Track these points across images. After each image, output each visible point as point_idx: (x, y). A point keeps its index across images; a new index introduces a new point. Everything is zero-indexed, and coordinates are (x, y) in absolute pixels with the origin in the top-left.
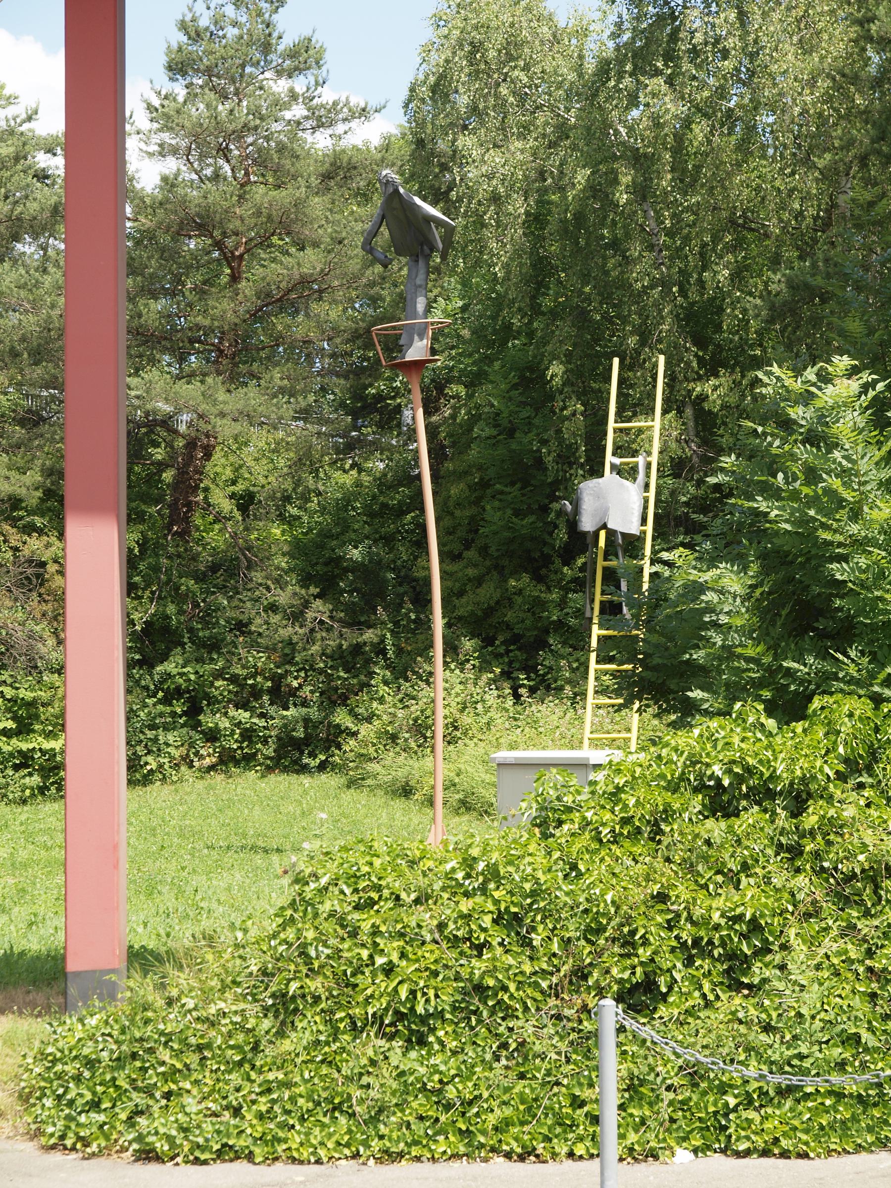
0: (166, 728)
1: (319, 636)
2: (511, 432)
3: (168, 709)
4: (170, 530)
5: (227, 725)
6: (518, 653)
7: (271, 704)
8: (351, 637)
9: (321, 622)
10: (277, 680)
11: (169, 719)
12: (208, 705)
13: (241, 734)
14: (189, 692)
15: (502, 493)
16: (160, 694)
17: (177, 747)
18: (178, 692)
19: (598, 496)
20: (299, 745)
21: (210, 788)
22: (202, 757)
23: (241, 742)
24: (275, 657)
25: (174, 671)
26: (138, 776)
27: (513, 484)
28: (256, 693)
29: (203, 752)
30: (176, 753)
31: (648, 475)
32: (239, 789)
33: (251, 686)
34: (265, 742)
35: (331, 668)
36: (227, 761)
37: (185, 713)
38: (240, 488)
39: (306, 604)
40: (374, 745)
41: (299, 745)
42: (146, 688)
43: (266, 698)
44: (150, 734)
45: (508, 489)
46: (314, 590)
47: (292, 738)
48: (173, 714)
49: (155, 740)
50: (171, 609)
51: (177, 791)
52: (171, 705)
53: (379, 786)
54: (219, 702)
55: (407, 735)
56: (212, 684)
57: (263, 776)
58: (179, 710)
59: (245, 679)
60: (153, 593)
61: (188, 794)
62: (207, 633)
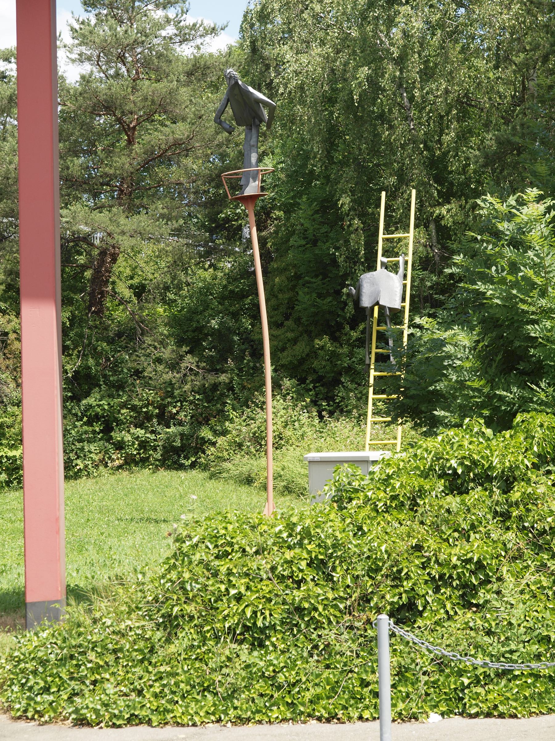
1: (189, 379)
2: (315, 243)
3: (91, 429)
4: (90, 310)
5: (130, 439)
6: (321, 388)
7: (159, 424)
8: (211, 379)
9: (191, 370)
12: (117, 425)
13: (139, 445)
14: (104, 417)
15: (309, 282)
16: (85, 419)
18: (97, 417)
19: (373, 283)
20: (177, 451)
21: (119, 480)
23: (139, 450)
25: (94, 404)
26: (71, 473)
27: (316, 276)
28: (149, 417)
29: (114, 457)
30: (96, 458)
31: (406, 269)
32: (138, 481)
33: (145, 412)
34: (155, 450)
36: (130, 462)
37: (101, 431)
38: (136, 281)
39: (181, 358)
40: (227, 450)
41: (177, 451)
42: (76, 415)
44: (79, 445)
45: (314, 280)
47: (173, 447)
48: (94, 432)
49: (82, 449)
50: (91, 362)
51: (97, 482)
53: (231, 478)
54: (124, 424)
55: (249, 444)
56: (119, 412)
57: (154, 472)
59: (141, 408)
62: (115, 378)
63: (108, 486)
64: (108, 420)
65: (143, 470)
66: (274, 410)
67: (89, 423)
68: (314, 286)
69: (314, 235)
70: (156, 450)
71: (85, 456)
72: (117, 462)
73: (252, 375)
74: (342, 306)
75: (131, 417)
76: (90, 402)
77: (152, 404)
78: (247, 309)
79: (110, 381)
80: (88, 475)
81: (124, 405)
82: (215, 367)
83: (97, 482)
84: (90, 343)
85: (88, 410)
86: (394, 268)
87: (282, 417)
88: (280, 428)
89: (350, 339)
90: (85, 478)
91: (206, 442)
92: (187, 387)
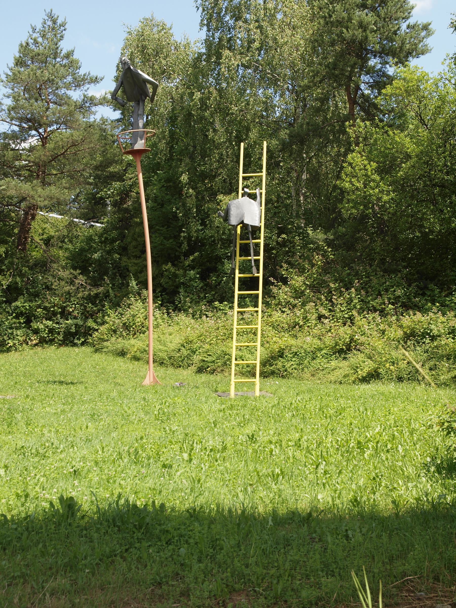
0: (17, 328)
1: (81, 290)
2: (162, 205)
3: (18, 321)
4: (17, 248)
5: (43, 327)
7: (61, 318)
8: (95, 291)
9: (82, 285)
10: (63, 308)
11: (18, 325)
12: (34, 319)
13: (48, 331)
14: (26, 314)
15: (159, 230)
16: (14, 315)
17: (21, 336)
19: (238, 207)
21: (36, 353)
22: (32, 340)
23: (49, 334)
24: (63, 299)
25: (20, 305)
26: (5, 348)
27: (163, 226)
29: (32, 338)
30: (21, 339)
31: (261, 197)
32: (48, 354)
33: (52, 311)
35: (86, 303)
36: (43, 342)
37: (24, 322)
38: (45, 236)
42: (8, 312)
43: (59, 316)
44: (10, 331)
46: (78, 271)
47: (70, 332)
48: (20, 323)
49: (12, 334)
50: (18, 279)
51: (21, 354)
52: (19, 319)
54: (39, 318)
55: (121, 330)
56: (36, 311)
57: (58, 348)
58: (22, 321)
59: (50, 308)
60: (11, 273)
61: (26, 356)
62: (33, 290)
66: (144, 308)
67: (17, 317)
68: (162, 232)
71: (14, 338)
72: (34, 341)
73: (120, 288)
74: (179, 245)
75: (43, 313)
80: (16, 350)
81: (39, 307)
86: (253, 197)
87: (142, 313)
88: (142, 320)
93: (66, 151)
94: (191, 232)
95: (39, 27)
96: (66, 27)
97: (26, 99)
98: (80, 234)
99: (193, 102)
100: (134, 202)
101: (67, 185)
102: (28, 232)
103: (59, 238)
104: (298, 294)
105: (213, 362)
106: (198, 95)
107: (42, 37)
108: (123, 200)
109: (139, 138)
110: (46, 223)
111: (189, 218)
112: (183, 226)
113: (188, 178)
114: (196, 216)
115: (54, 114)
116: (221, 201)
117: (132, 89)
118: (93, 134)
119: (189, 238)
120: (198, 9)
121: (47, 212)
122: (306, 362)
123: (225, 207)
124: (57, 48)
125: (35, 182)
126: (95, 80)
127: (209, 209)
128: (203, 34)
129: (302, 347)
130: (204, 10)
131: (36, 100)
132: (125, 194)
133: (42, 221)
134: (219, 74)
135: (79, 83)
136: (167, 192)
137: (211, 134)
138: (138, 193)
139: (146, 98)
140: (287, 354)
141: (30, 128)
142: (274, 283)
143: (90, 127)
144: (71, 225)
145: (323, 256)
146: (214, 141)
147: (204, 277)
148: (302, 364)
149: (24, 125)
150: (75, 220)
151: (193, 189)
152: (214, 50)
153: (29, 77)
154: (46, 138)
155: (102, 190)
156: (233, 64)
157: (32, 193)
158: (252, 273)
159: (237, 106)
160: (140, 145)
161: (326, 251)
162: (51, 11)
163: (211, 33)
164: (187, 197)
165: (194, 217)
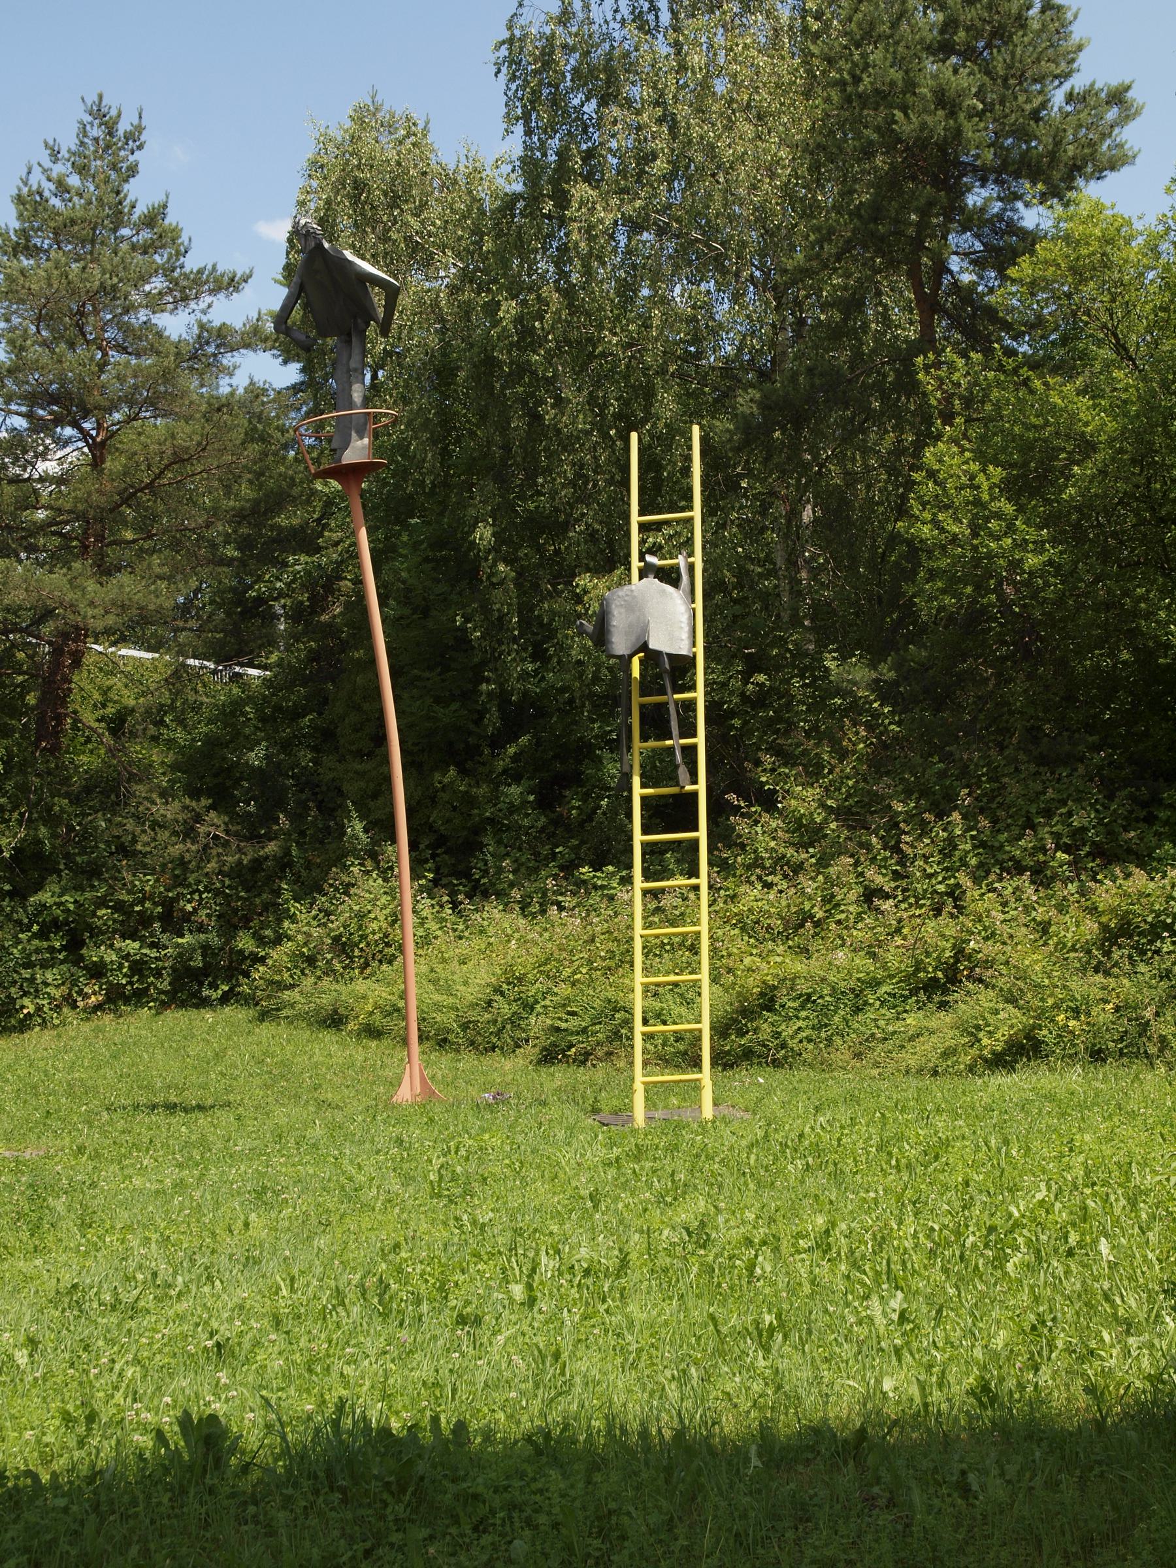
0: (45, 965)
1: (214, 852)
2: (426, 613)
3: (45, 944)
4: (37, 747)
5: (114, 958)
9: (216, 837)
13: (130, 968)
16: (35, 927)
19: (632, 606)
20: (198, 976)
21: (98, 1030)
25: (50, 901)
28: (145, 920)
30: (56, 993)
36: (116, 999)
37: (64, 948)
38: (110, 710)
40: (289, 969)
41: (198, 976)
42: (19, 923)
44: (26, 974)
47: (189, 969)
48: (52, 950)
49: (32, 979)
50: (43, 831)
51: (59, 1036)
53: (297, 1017)
54: (103, 934)
55: (329, 956)
56: (94, 914)
57: (158, 1014)
59: (132, 905)
63: (80, 1042)
64: (75, 929)
65: (140, 1011)
66: (389, 894)
67: (43, 935)
69: (424, 599)
70: (161, 975)
71: (37, 991)
72: (93, 998)
75: (114, 921)
76: (43, 900)
77: (151, 898)
78: (304, 736)
79: (76, 863)
82: (255, 829)
83: (59, 1036)
84: (40, 800)
85: (40, 913)
86: (669, 576)
88: (384, 925)
89: (491, 772)
90: (37, 1029)
91: (246, 958)
92: (212, 866)
93: (159, 476)
94: (507, 681)
95: (68, 141)
96: (142, 138)
97: (44, 343)
98: (205, 699)
99: (498, 329)
100: (348, 606)
101: (166, 569)
102: (63, 702)
103: (148, 712)
104: (806, 833)
105: (584, 1031)
106: (509, 309)
107: (80, 173)
108: (318, 603)
109: (354, 434)
110: (112, 673)
111: (500, 643)
112: (483, 664)
113: (493, 535)
114: (521, 636)
115: (120, 378)
116: (586, 592)
117: (326, 302)
118: (230, 429)
119: (503, 697)
120: (499, 71)
121: (114, 644)
122: (836, 1019)
123: (595, 607)
124: (120, 203)
125: (77, 565)
126: (231, 284)
127: (553, 613)
128: (515, 145)
129: (823, 980)
130: (513, 78)
131: (72, 345)
132: (323, 586)
133: (101, 669)
134: (563, 249)
135: (185, 289)
136: (432, 579)
137: (549, 413)
138: (359, 581)
139: (368, 325)
140: (785, 999)
141: (58, 421)
142: (740, 807)
143: (219, 410)
144: (179, 674)
145: (870, 727)
146: (559, 431)
147: (547, 800)
148: (826, 1025)
149: (41, 412)
150: (191, 662)
151: (507, 562)
152: (547, 182)
153: (50, 285)
154: (103, 442)
155: (259, 579)
156: (601, 221)
157: (70, 596)
158: (677, 784)
159: (615, 334)
160: (358, 451)
161: (876, 715)
162: (101, 97)
163: (535, 139)
164: (493, 585)
165: (515, 640)
